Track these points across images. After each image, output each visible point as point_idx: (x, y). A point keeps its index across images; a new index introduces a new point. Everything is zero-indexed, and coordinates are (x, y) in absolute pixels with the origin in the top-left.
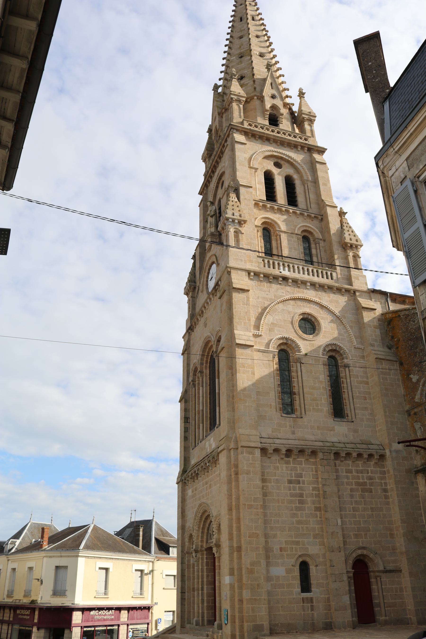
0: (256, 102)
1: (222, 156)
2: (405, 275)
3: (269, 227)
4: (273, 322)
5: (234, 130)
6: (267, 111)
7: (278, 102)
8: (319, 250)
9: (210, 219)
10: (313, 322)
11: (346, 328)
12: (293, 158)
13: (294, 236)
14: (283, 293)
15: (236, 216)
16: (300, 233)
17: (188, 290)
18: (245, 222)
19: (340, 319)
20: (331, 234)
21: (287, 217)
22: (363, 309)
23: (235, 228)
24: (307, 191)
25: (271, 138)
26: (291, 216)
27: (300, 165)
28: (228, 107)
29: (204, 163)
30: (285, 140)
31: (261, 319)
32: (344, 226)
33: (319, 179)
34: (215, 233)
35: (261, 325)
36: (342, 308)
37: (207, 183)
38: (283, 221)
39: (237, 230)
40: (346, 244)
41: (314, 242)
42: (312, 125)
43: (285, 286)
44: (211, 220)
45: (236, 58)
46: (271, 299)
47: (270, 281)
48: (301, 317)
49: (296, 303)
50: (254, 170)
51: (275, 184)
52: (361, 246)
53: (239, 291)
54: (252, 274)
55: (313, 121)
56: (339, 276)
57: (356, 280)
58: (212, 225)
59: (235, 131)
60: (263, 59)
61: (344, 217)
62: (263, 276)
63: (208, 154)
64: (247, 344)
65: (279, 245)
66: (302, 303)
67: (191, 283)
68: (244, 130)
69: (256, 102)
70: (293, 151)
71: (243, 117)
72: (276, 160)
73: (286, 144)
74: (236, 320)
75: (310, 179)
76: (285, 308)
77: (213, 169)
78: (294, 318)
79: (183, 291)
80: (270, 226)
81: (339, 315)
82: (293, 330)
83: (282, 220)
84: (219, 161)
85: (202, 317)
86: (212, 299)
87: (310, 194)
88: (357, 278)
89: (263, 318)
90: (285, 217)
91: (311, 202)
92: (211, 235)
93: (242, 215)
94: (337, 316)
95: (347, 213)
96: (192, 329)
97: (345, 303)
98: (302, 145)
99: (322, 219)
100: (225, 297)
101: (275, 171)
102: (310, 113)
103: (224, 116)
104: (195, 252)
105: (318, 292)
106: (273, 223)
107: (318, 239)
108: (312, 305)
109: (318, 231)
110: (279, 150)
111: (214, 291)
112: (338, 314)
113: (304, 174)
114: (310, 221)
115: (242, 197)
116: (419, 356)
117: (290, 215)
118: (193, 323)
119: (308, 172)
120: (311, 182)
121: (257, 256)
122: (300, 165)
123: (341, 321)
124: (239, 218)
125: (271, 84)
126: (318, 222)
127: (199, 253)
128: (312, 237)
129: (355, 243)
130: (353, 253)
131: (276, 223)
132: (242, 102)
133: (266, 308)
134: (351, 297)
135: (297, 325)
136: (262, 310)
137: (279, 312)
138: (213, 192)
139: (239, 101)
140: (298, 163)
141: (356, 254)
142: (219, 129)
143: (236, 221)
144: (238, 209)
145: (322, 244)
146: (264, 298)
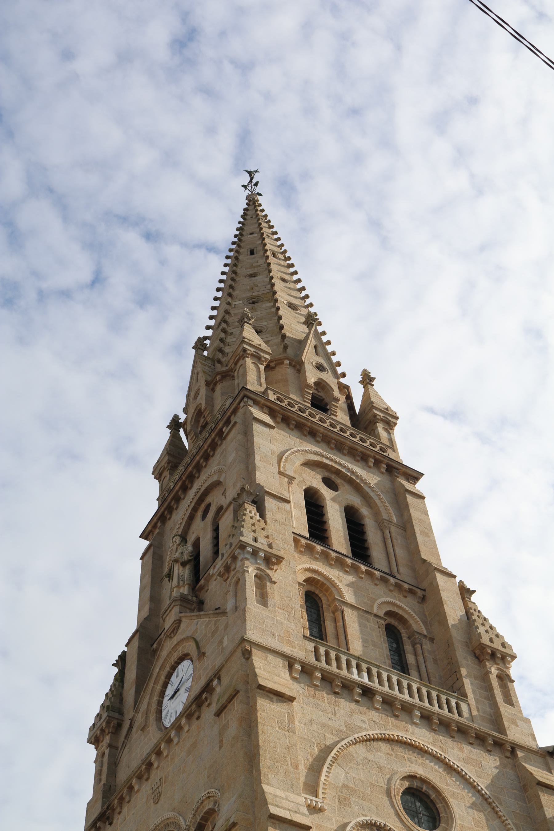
0: (286, 371)
1: (211, 454)
3: (317, 592)
4: (346, 783)
5: (249, 400)
6: (308, 386)
7: (328, 377)
8: (422, 657)
9: (179, 570)
10: (432, 801)
11: (505, 826)
12: (361, 476)
13: (372, 618)
14: (363, 722)
15: (263, 544)
16: (382, 616)
17: (102, 731)
18: (280, 559)
19: (490, 804)
20: (450, 624)
21: (354, 579)
22: (539, 788)
23: (258, 569)
24: (389, 542)
25: (318, 431)
26: (362, 578)
27: (373, 491)
28: (233, 366)
30: (344, 441)
31: (319, 772)
32: (472, 614)
33: (414, 522)
34: (190, 597)
35: (321, 786)
36: (492, 781)
37: (166, 513)
38: (348, 585)
39: (261, 573)
40: (483, 647)
41: (409, 641)
42: (390, 431)
43: (369, 709)
45: (243, 303)
46: (339, 731)
47: (337, 690)
48: (407, 784)
49: (393, 750)
50: (287, 480)
51: (326, 517)
52: (514, 657)
53: (272, 696)
54: (298, 667)
55: (393, 424)
56: (475, 713)
57: (513, 726)
58: (183, 581)
59: (251, 402)
60: (295, 313)
61: (470, 599)
62: (320, 676)
63: (169, 462)
64: (295, 819)
65: (341, 631)
66: (405, 753)
67: (112, 714)
68: (268, 404)
69: (286, 371)
70: (359, 464)
71: (264, 386)
72: (327, 474)
73: (347, 448)
74: (265, 762)
75: (395, 521)
76: (371, 757)
77: (187, 483)
78: (393, 783)
80: (320, 590)
81: (488, 793)
82: (392, 811)
83: (346, 582)
84: (204, 465)
85: (147, 779)
86: (186, 728)
87: (396, 548)
88: (514, 722)
89: (325, 769)
90: (351, 578)
91: (399, 563)
92: (180, 600)
93: (274, 546)
94: (482, 795)
95: (474, 592)
96: (108, 818)
97: (496, 771)
98: (377, 457)
99: (424, 596)
100: (237, 707)
101: (326, 492)
102: (387, 409)
103: (218, 388)
104: (124, 653)
105: (438, 734)
106: (328, 584)
107: (420, 634)
108: (428, 762)
109: (418, 619)
110: (333, 457)
111: (194, 707)
112: (485, 791)
113: (382, 509)
114: (401, 596)
115: (269, 515)
117: (361, 576)
118: (116, 802)
119: (389, 508)
120: (397, 526)
121: (304, 636)
122: (373, 491)
123: (493, 808)
124: (266, 548)
125: (316, 347)
126: (415, 603)
127: (137, 648)
128: (404, 629)
129: (501, 648)
130: (498, 669)
131: (334, 585)
132: (263, 361)
133: (328, 750)
134: (507, 759)
135: (398, 801)
136: (321, 751)
137: (357, 764)
138: (181, 523)
139: (258, 358)
140: (370, 487)
141: (504, 674)
142: (206, 409)
143: (262, 554)
144: (263, 533)
145: (427, 646)
146: (324, 725)
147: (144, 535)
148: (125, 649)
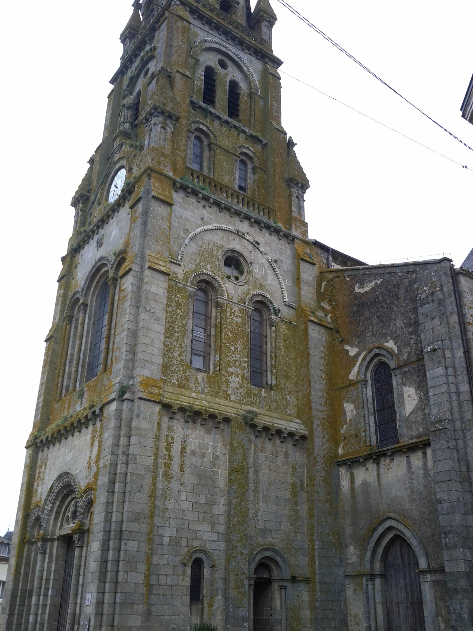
2: (450, 133)
29: (122, 44)
44: (127, 114)
63: (130, 33)
79: (70, 202)
95: (296, 144)
100: (140, 208)
116: (363, 325)
147: (112, 82)
148: (95, 154)
